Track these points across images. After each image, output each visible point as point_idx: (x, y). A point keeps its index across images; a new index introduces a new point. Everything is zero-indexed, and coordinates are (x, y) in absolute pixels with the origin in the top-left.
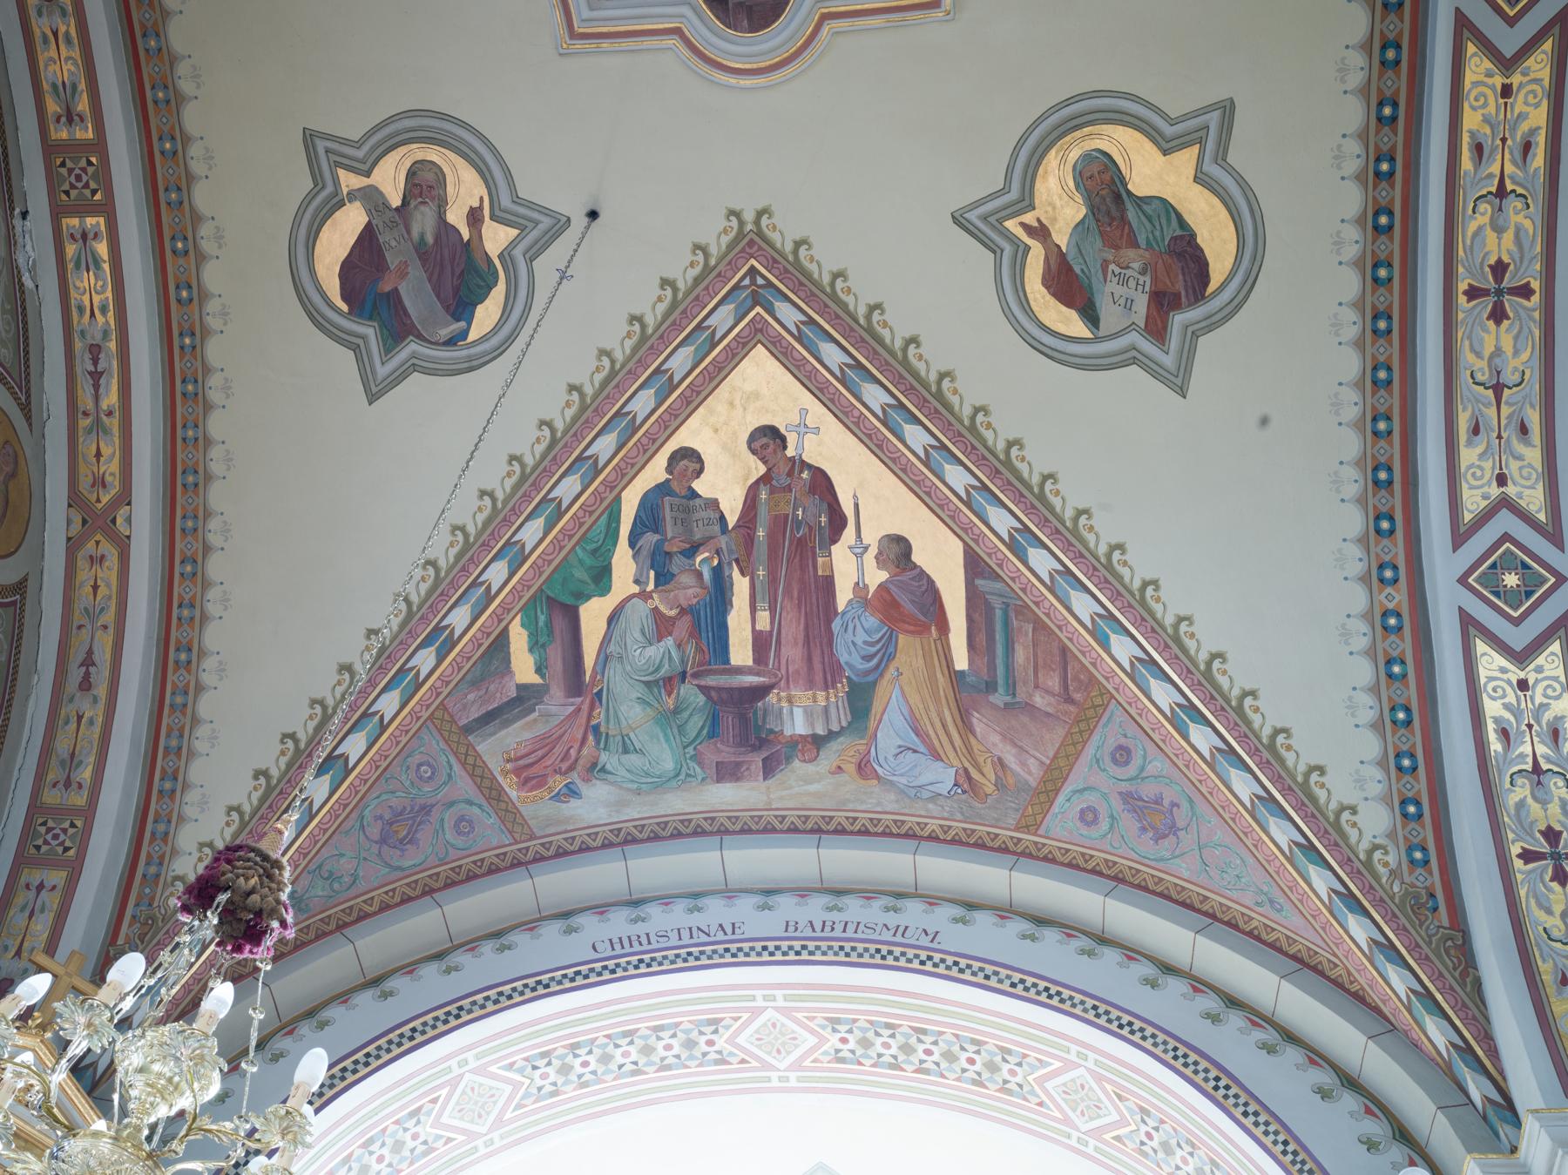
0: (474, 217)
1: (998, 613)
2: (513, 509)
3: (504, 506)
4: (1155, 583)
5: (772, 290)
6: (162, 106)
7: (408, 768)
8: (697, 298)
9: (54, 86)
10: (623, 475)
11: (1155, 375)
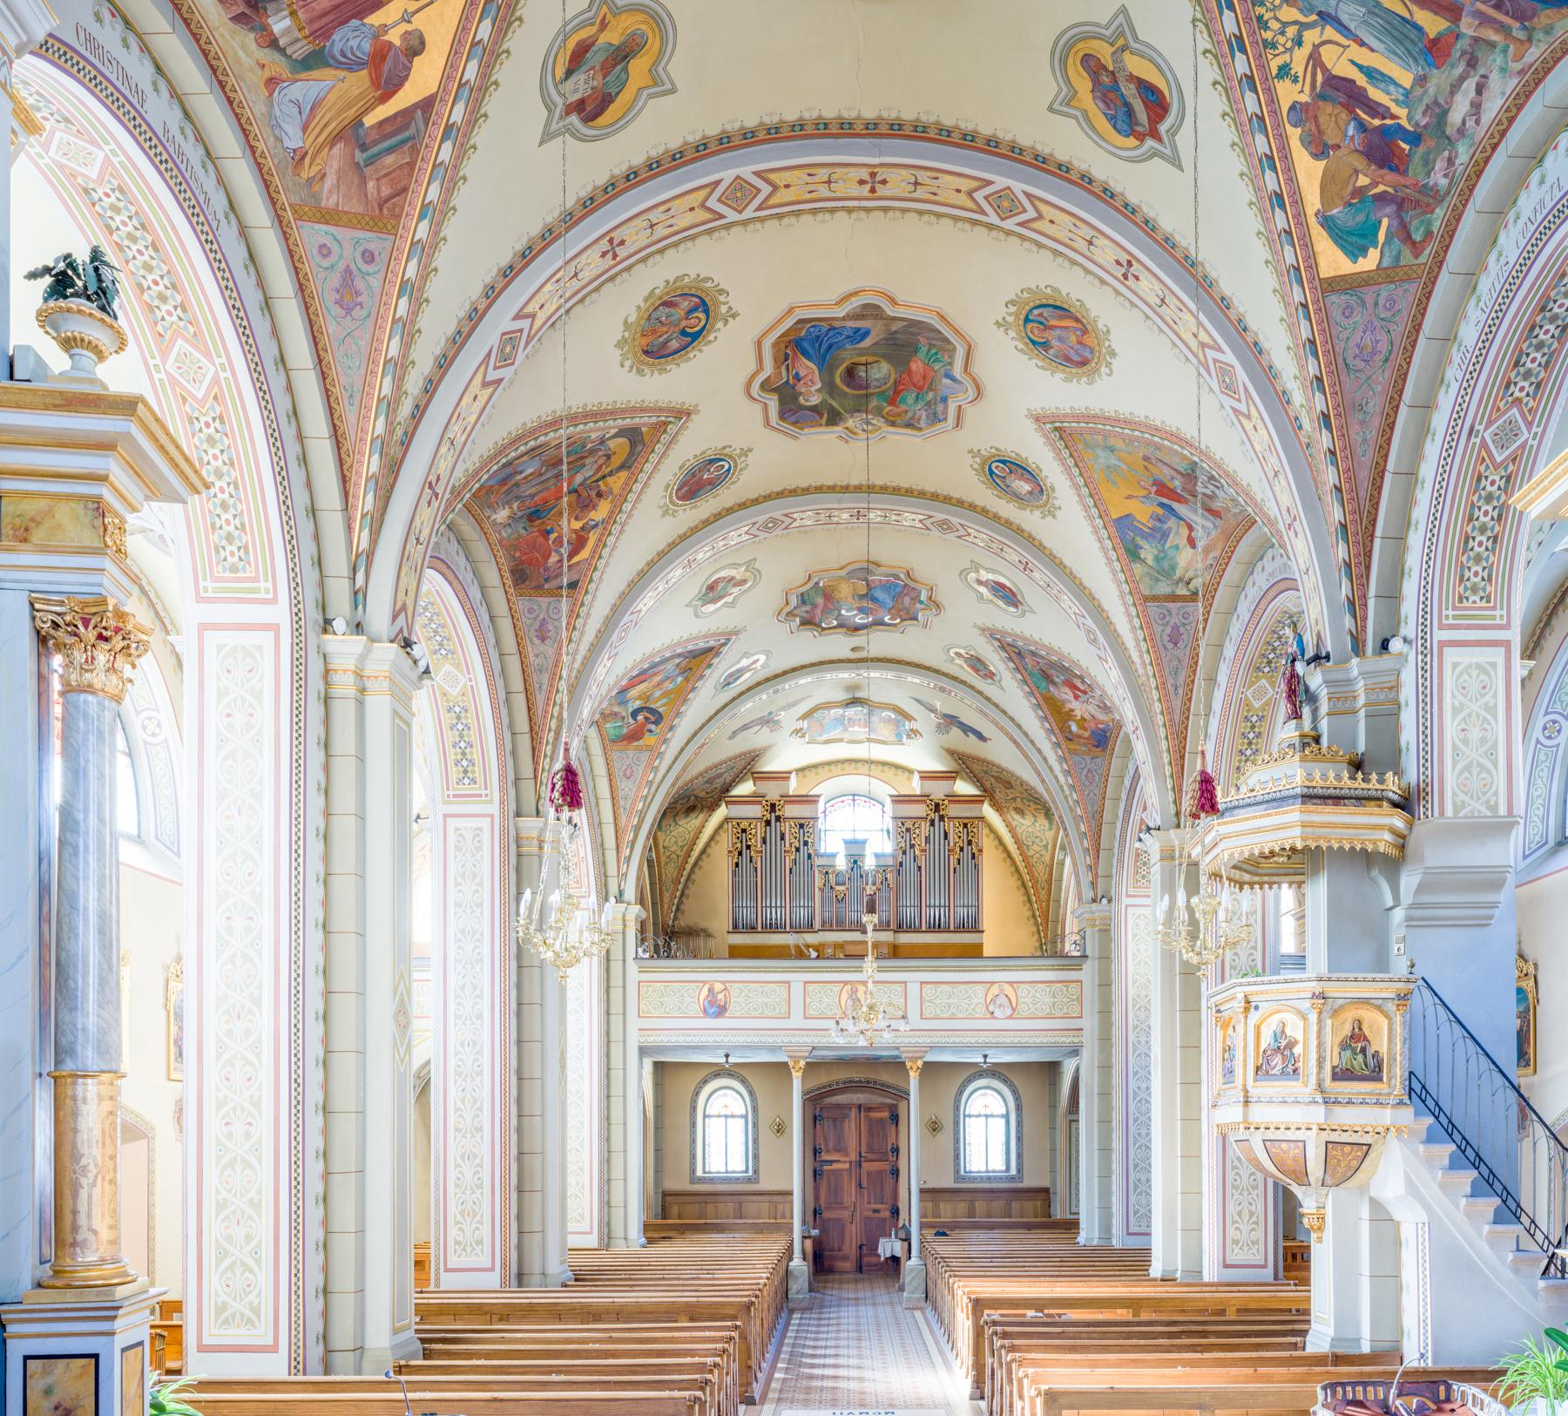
1: (407, 134)
11: (546, 125)
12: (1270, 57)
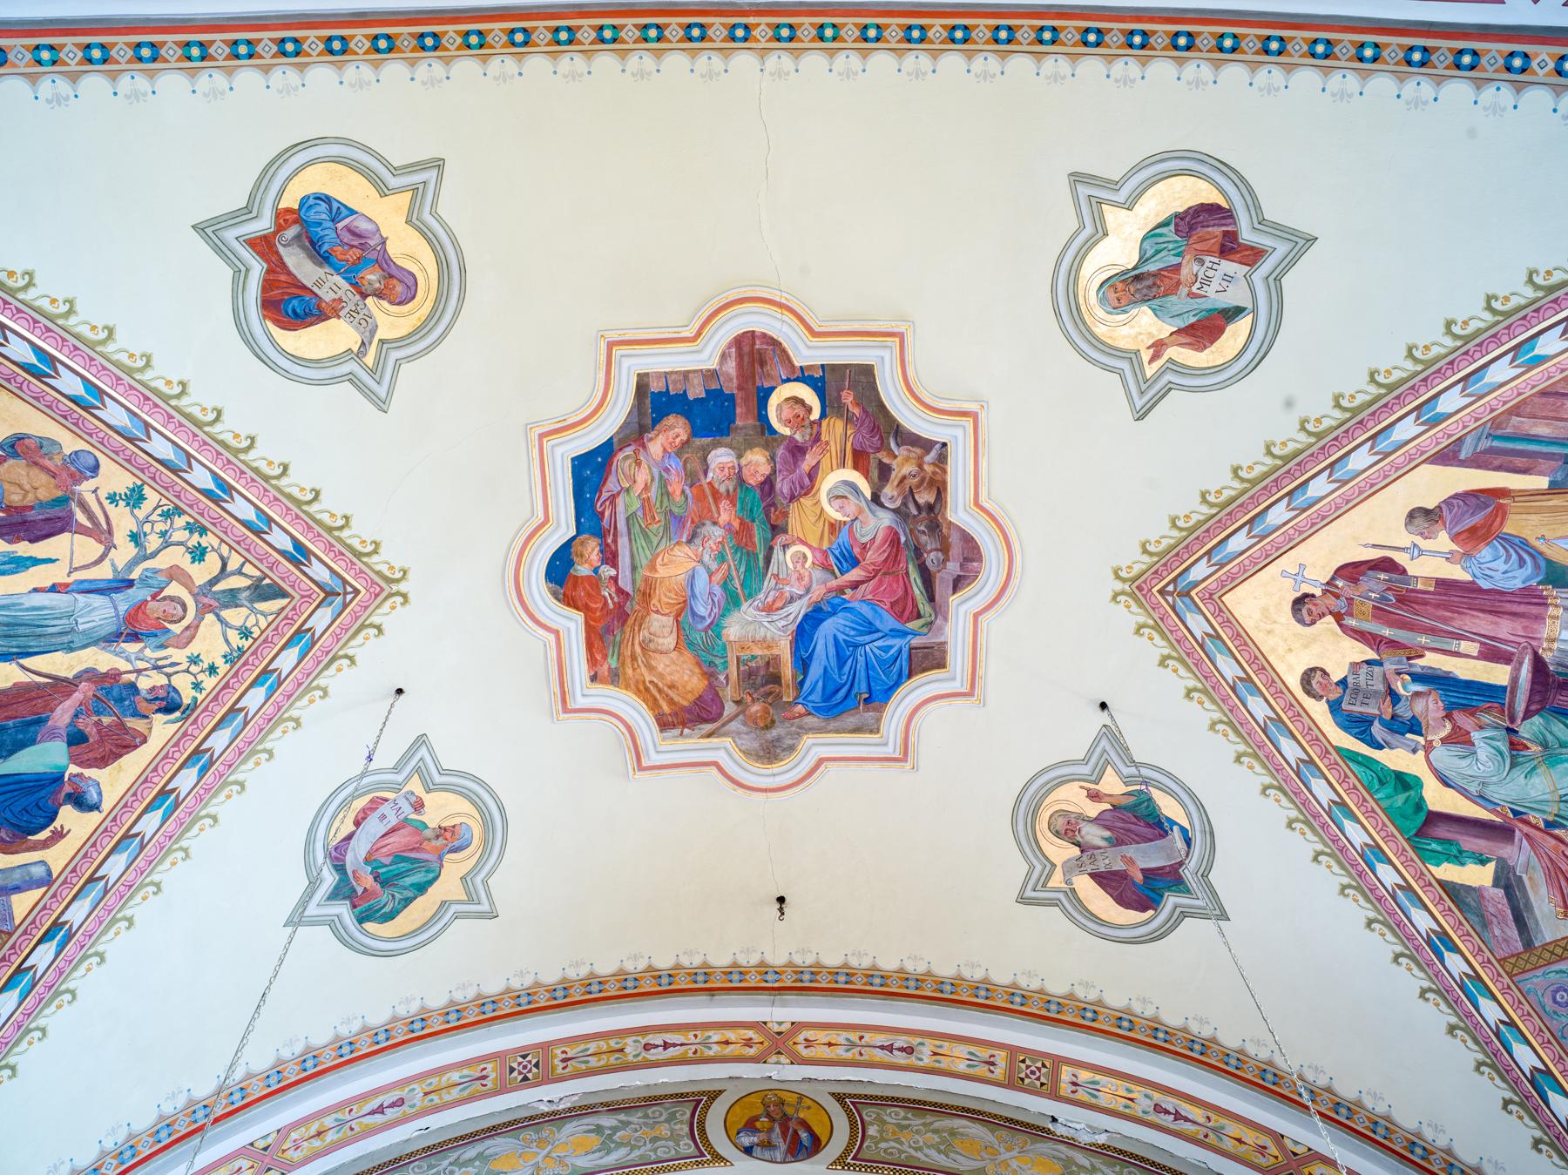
0: (1095, 796)
1: (1496, 444)
2: (1333, 841)
3: (1330, 847)
4: (1489, 298)
5: (1179, 580)
6: (990, 995)
7: (1555, 1013)
8: (1178, 641)
9: (969, 1066)
10: (1317, 739)
12: (164, 501)
